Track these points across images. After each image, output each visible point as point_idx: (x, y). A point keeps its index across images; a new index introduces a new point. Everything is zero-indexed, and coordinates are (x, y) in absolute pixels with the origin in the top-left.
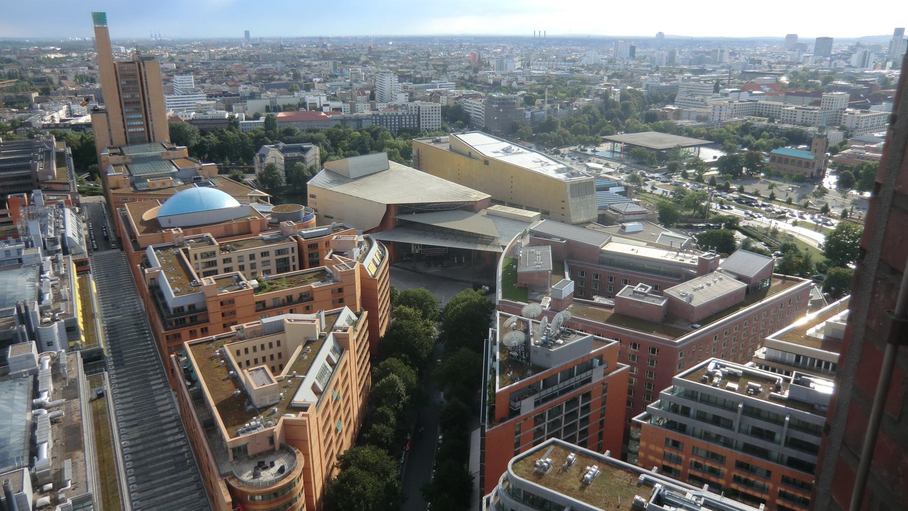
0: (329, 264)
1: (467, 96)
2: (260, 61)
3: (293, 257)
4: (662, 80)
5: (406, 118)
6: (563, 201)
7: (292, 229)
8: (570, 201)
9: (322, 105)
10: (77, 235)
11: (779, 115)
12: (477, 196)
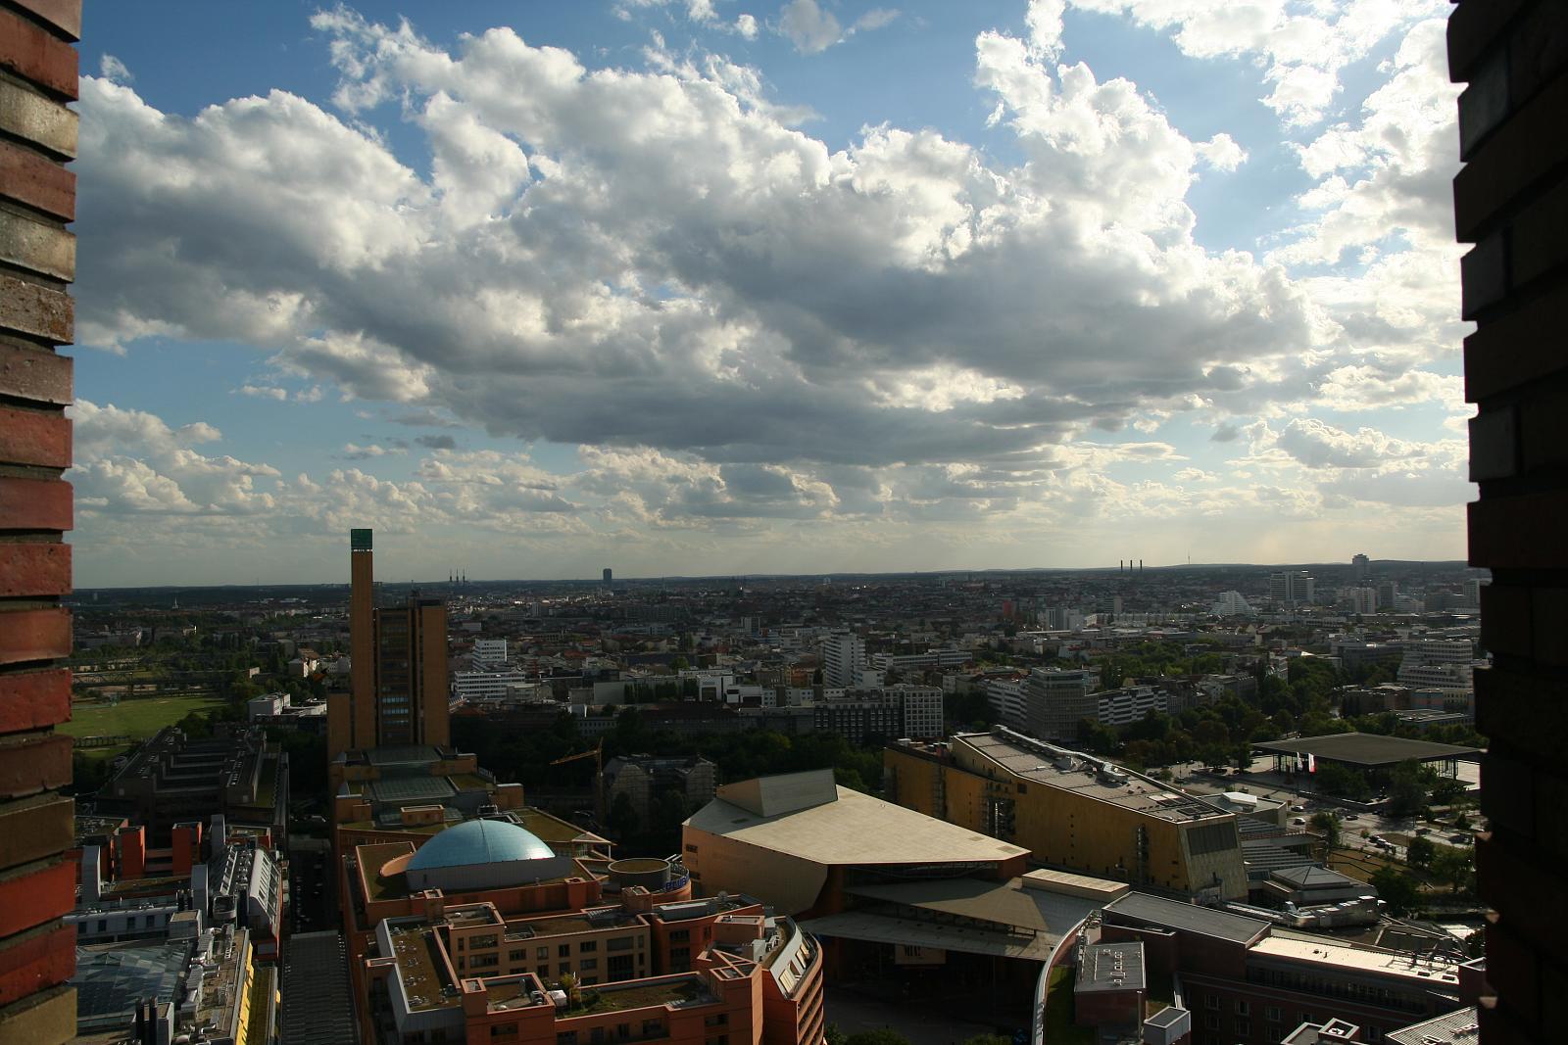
0: (704, 966)
1: (992, 676)
2: (625, 619)
3: (641, 956)
4: (1369, 638)
5: (877, 716)
6: (1175, 863)
7: (642, 902)
8: (1188, 863)
9: (725, 691)
10: (266, 896)
12: (992, 849)
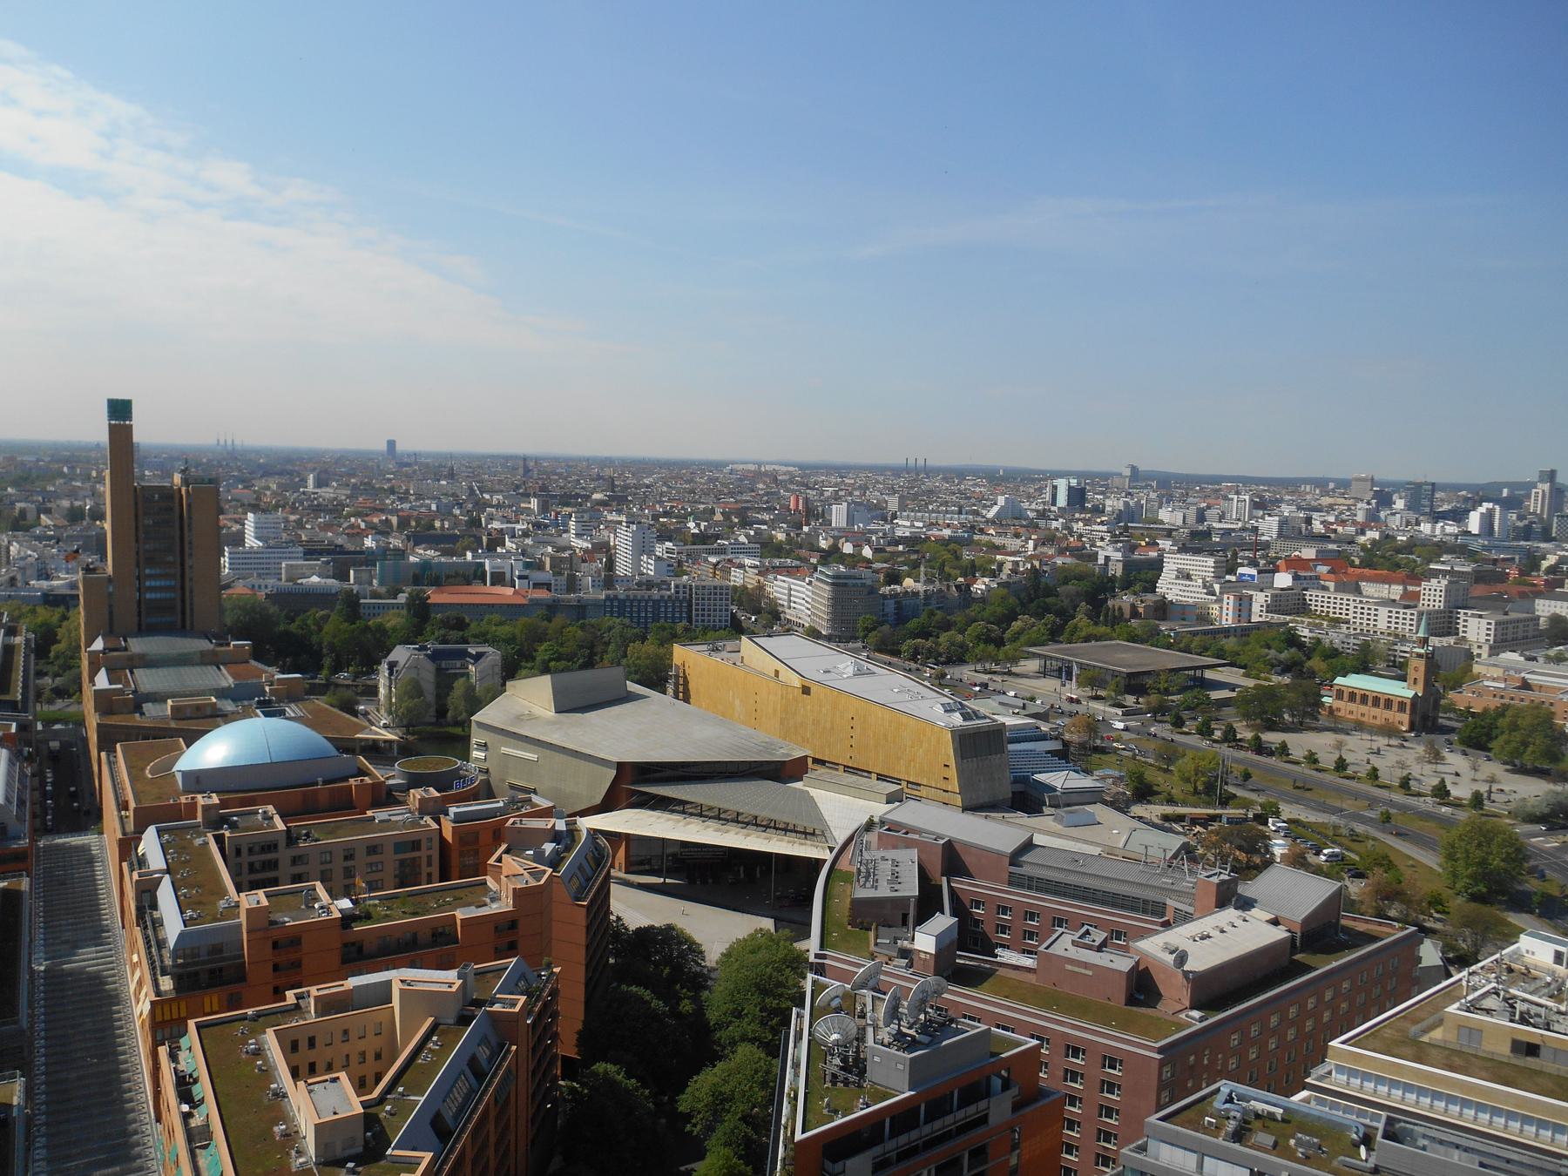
3: (429, 857)
5: (666, 607)
11: (1347, 614)
